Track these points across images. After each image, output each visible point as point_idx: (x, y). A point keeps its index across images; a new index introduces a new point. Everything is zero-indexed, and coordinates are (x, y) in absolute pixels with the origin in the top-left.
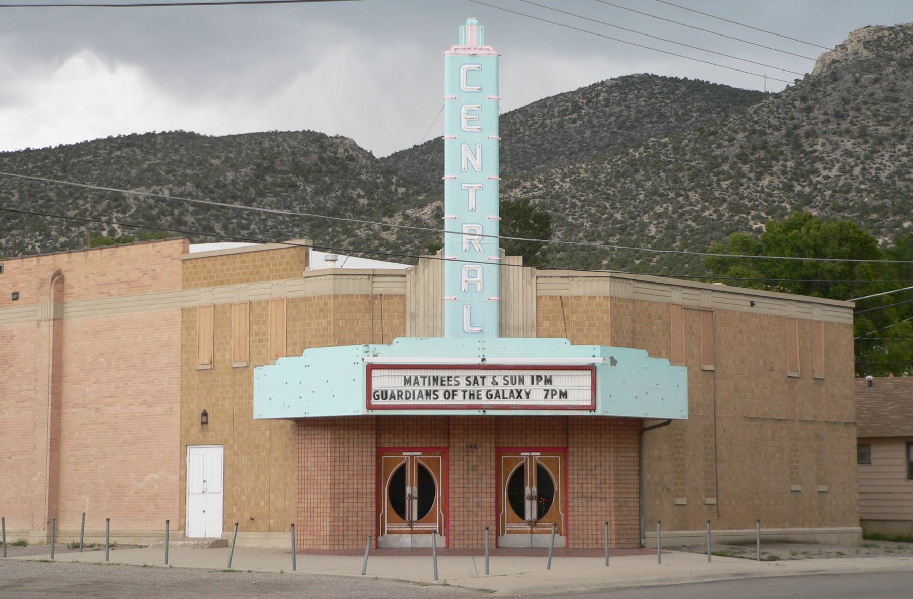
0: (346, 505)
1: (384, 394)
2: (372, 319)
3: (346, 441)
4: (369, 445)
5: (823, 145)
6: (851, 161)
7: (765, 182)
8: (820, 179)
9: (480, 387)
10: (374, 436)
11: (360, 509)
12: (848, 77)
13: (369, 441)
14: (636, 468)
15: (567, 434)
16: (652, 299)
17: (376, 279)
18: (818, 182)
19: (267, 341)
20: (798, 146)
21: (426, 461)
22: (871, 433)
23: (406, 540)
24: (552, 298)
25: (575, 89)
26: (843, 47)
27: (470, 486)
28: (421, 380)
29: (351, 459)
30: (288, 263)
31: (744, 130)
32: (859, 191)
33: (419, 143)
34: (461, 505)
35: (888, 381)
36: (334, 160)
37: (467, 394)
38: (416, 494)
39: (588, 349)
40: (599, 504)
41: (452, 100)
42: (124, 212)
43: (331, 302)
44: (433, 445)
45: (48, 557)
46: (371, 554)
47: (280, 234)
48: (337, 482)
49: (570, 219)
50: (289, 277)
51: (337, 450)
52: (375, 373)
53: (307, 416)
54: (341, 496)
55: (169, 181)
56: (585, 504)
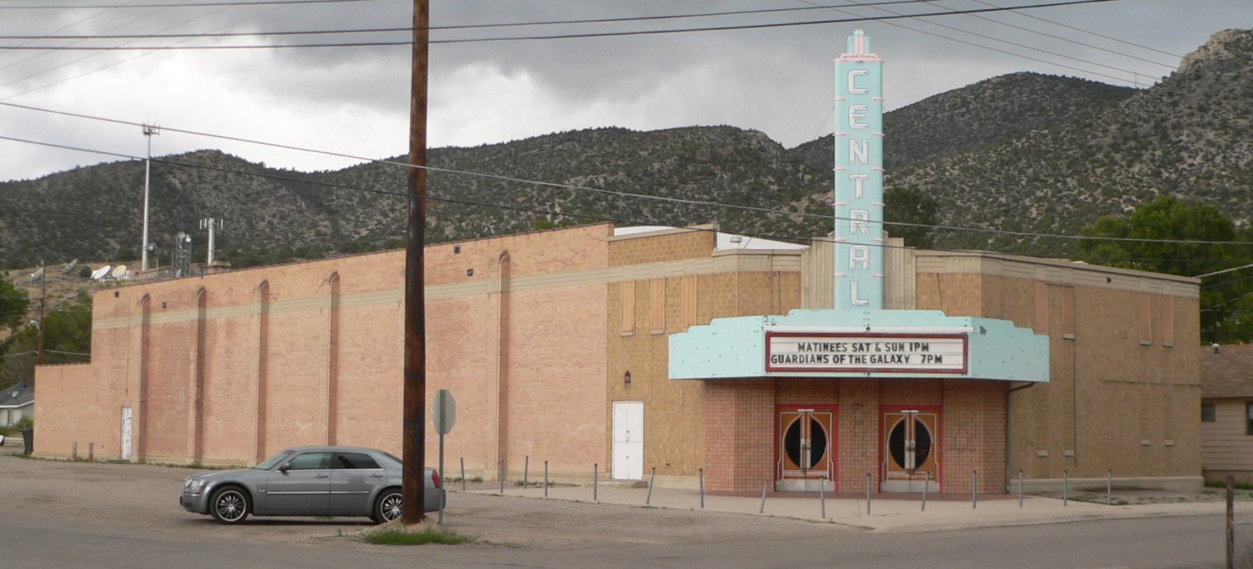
2: (769, 292)
5: (1188, 136)
6: (1213, 150)
7: (1136, 169)
8: (1185, 166)
12: (1210, 74)
16: (1019, 275)
18: (1184, 169)
20: (1165, 137)
21: (819, 416)
22: (1215, 393)
23: (801, 485)
25: (963, 86)
26: (1205, 47)
27: (856, 439)
31: (1116, 122)
32: (1220, 177)
33: (824, 136)
35: (1232, 349)
36: (748, 151)
38: (809, 445)
39: (961, 320)
41: (840, 99)
42: (565, 198)
45: (498, 492)
46: (769, 495)
47: (700, 216)
49: (959, 203)
50: (699, 256)
52: (773, 340)
55: (604, 171)
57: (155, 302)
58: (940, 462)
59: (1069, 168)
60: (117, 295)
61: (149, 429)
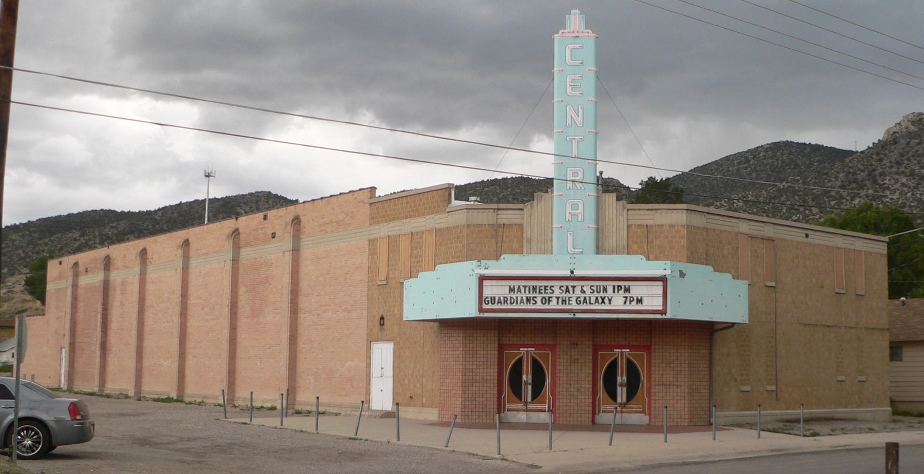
1: (493, 301)
9: (571, 295)
12: (903, 141)
14: (708, 362)
16: (722, 228)
17: (500, 212)
20: (875, 181)
21: (539, 355)
22: (902, 338)
23: (522, 417)
24: (640, 226)
26: (899, 124)
31: (844, 172)
32: (910, 207)
37: (560, 300)
38: (530, 381)
45: (248, 421)
50: (437, 212)
52: (485, 283)
57: (81, 268)
58: (649, 396)
59: (813, 201)
60: (60, 263)
61: (76, 365)
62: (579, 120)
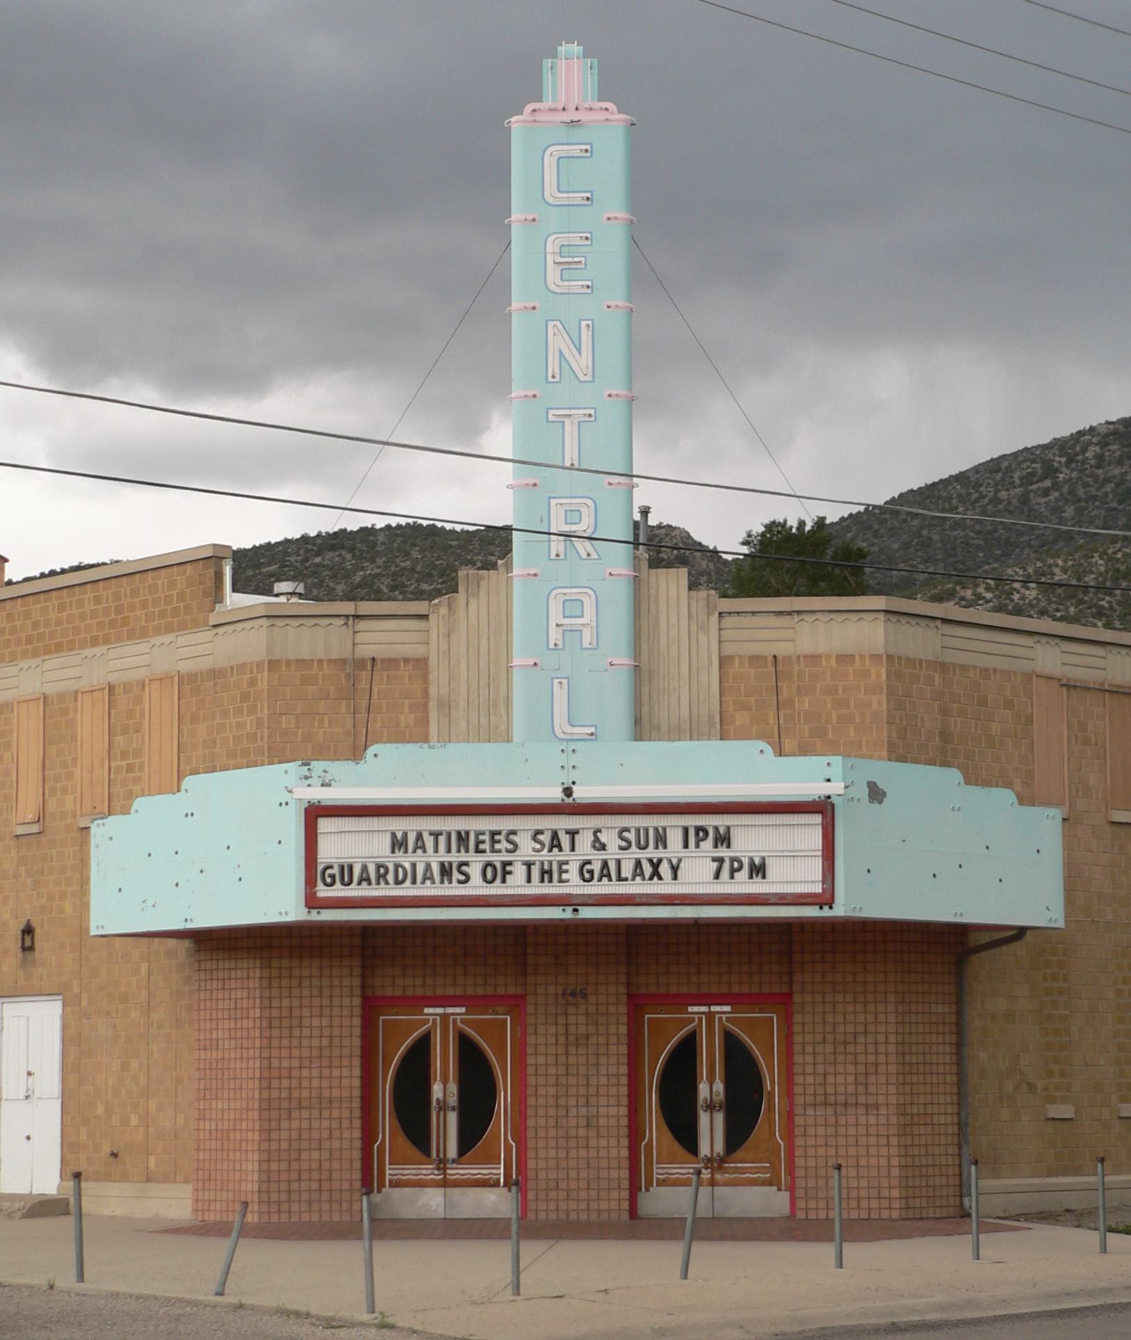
0: (295, 1124)
1: (346, 874)
3: (295, 982)
4: (346, 991)
10: (357, 971)
11: (325, 1134)
13: (346, 982)
15: (791, 962)
16: (990, 662)
17: (362, 625)
19: (142, 769)
23: (433, 1202)
24: (755, 660)
28: (429, 841)
29: (306, 1022)
30: (181, 597)
34: (552, 1122)
37: (536, 871)
38: (453, 1100)
40: (862, 1120)
43: (263, 678)
44: (490, 991)
48: (275, 1073)
50: (183, 627)
51: (276, 1003)
52: (324, 825)
53: (190, 926)
54: (285, 1104)
56: (831, 1120)
62: (582, 363)
